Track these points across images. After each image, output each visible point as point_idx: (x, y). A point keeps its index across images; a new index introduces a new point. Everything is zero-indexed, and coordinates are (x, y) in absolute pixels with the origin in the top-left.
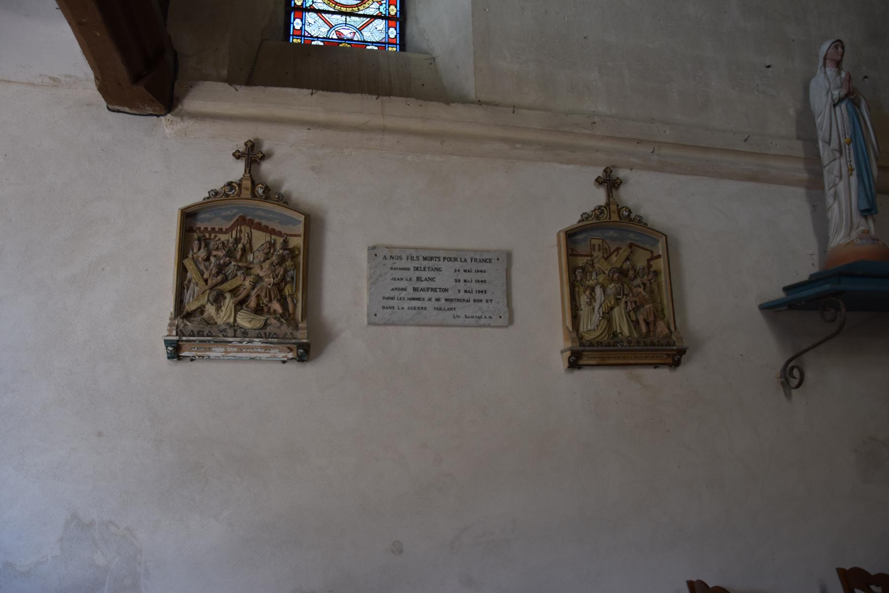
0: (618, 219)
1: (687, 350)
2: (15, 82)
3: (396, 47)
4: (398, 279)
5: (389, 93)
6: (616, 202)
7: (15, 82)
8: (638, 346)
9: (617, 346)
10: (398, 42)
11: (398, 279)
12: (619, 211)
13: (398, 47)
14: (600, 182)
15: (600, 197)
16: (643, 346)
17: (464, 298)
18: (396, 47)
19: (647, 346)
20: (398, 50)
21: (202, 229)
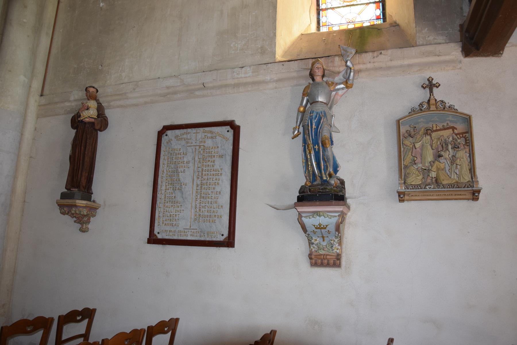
0: (435, 109)
1: (481, 191)
2: (20, 145)
3: (381, 21)
4: (463, 195)
5: (368, 52)
6: (435, 99)
7: (20, 145)
8: (438, 188)
9: (427, 189)
10: (382, 17)
11: (463, 195)
12: (436, 103)
13: (382, 20)
14: (425, 87)
15: (422, 95)
16: (442, 188)
17: (211, 131)
18: (381, 21)
19: (445, 188)
20: (382, 22)
21: (216, 133)
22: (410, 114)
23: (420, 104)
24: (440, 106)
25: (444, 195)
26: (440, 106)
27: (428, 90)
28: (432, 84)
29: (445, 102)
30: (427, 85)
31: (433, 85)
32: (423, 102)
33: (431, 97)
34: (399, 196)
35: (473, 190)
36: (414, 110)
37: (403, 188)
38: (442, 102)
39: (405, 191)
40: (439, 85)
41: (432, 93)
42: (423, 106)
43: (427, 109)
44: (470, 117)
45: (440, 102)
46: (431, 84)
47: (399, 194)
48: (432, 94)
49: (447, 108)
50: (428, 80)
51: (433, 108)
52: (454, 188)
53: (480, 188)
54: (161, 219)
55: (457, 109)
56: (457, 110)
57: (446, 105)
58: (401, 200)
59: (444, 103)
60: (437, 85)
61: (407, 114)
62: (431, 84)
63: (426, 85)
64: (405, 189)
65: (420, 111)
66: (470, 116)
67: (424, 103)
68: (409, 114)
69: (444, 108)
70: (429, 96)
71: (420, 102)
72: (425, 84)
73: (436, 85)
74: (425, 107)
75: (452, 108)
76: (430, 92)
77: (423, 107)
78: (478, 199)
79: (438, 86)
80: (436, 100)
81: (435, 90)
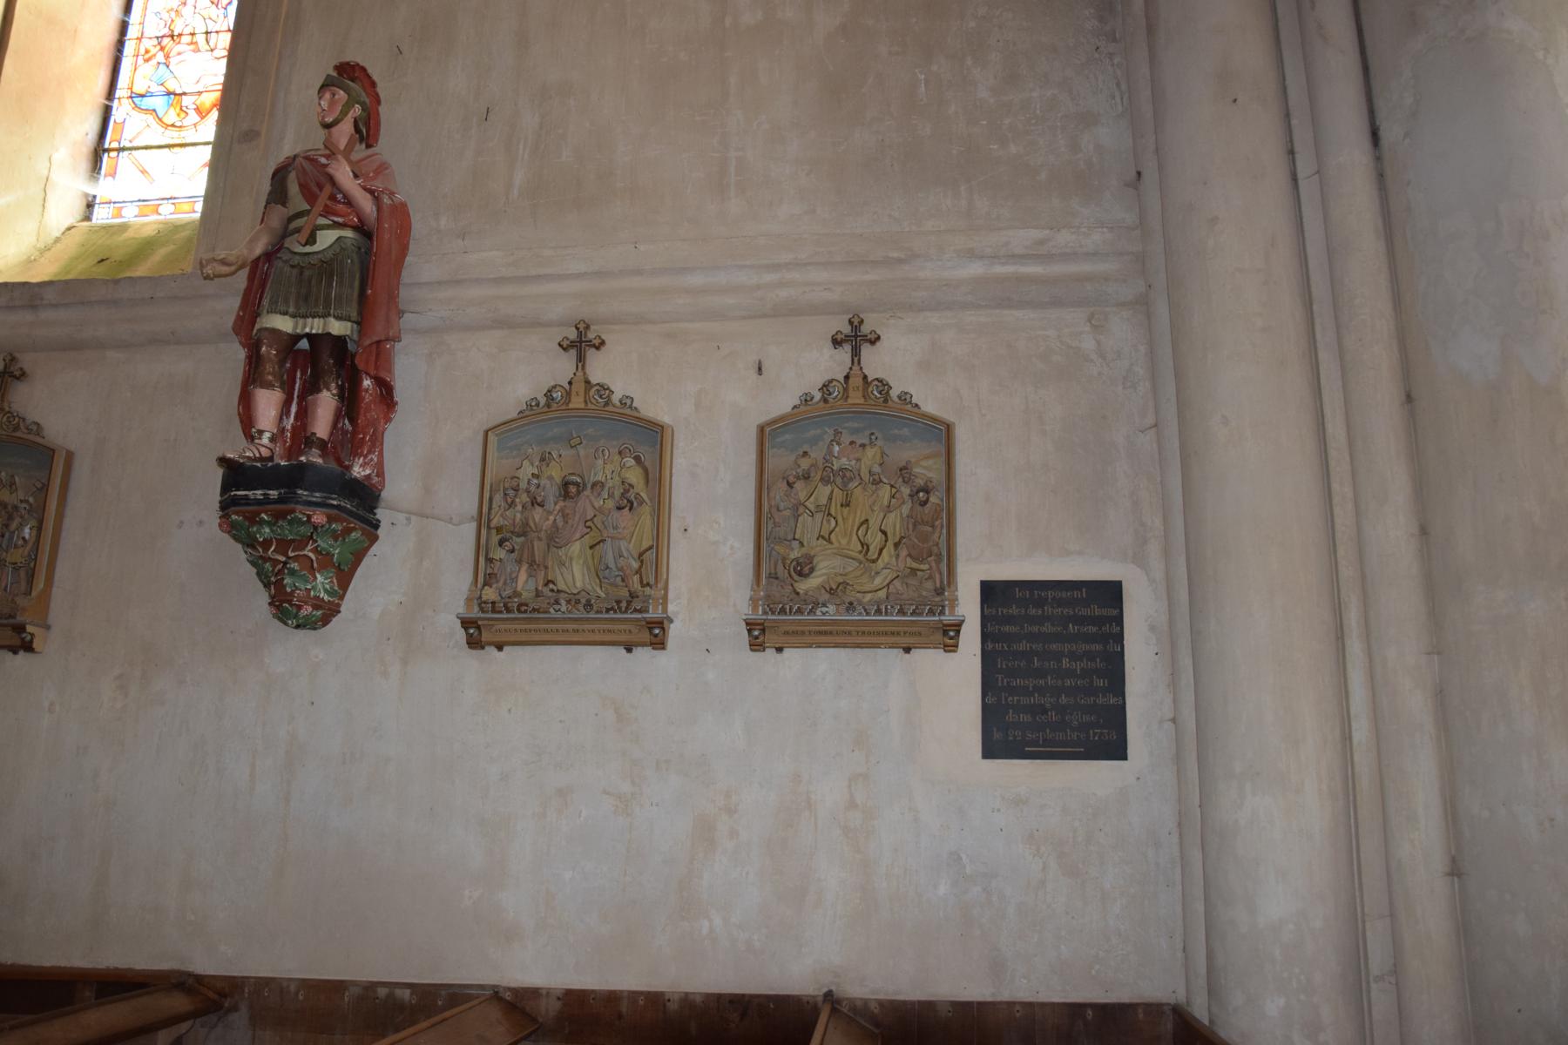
9: (550, 612)
16: (860, 614)
22: (796, 410)
23: (824, 386)
24: (875, 393)
25: (907, 634)
26: (875, 393)
27: (573, 352)
28: (583, 339)
29: (887, 384)
30: (846, 336)
31: (587, 341)
32: (831, 381)
33: (854, 368)
34: (749, 631)
35: (941, 621)
36: (806, 400)
37: (760, 613)
38: (880, 384)
39: (765, 620)
40: (876, 336)
41: (580, 362)
42: (831, 390)
43: (841, 399)
44: (949, 428)
45: (876, 383)
46: (856, 332)
47: (750, 625)
48: (856, 359)
49: (893, 401)
50: (851, 322)
51: (856, 398)
52: (626, 612)
53: (961, 618)
54: (1048, 701)
55: (638, 408)
56: (917, 405)
57: (891, 392)
58: (756, 645)
59: (607, 392)
60: (597, 342)
61: (514, 415)
62: (856, 332)
63: (568, 342)
64: (765, 613)
65: (822, 404)
66: (948, 426)
67: (834, 383)
68: (793, 409)
69: (886, 401)
70: (850, 365)
71: (823, 382)
72: (568, 339)
73: (594, 341)
74: (836, 393)
75: (905, 399)
76: (852, 356)
77: (830, 394)
78: (956, 646)
79: (874, 340)
80: (865, 377)
81: (866, 350)
